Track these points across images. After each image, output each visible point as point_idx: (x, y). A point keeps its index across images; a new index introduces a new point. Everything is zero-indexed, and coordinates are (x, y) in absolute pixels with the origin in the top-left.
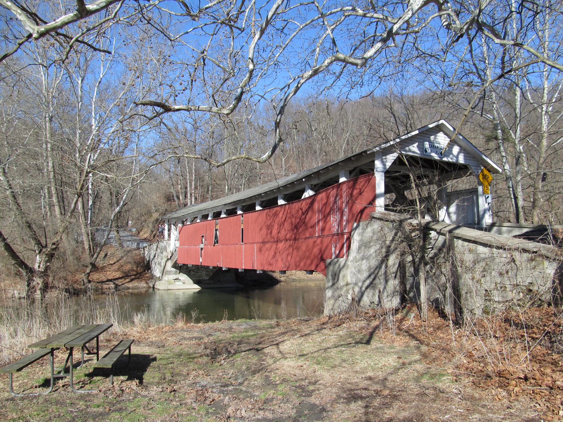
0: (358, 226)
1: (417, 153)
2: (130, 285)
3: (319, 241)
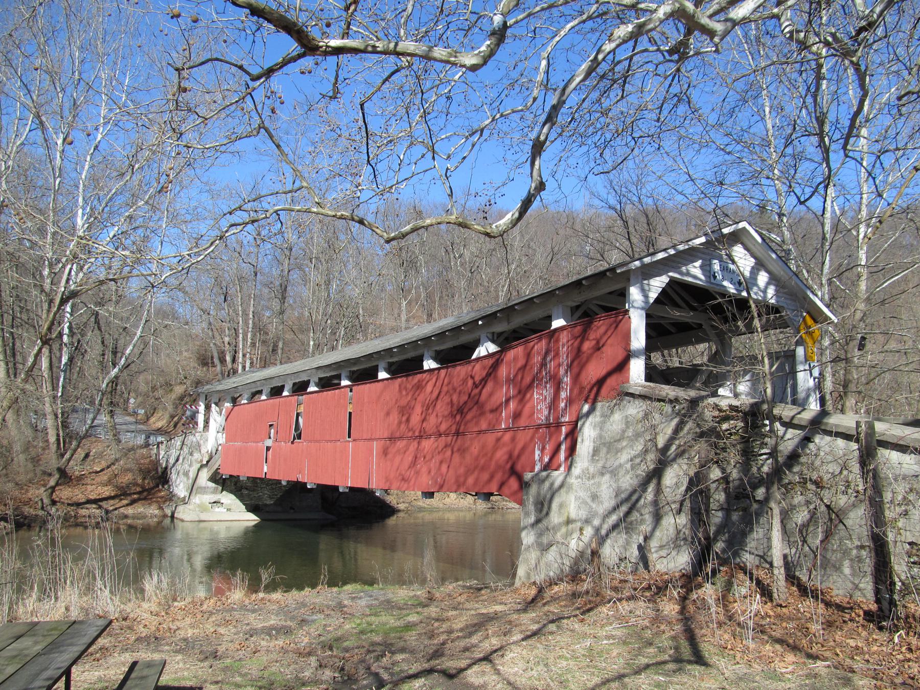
0: (592, 410)
1: (700, 280)
2: (130, 511)
3: (507, 437)
